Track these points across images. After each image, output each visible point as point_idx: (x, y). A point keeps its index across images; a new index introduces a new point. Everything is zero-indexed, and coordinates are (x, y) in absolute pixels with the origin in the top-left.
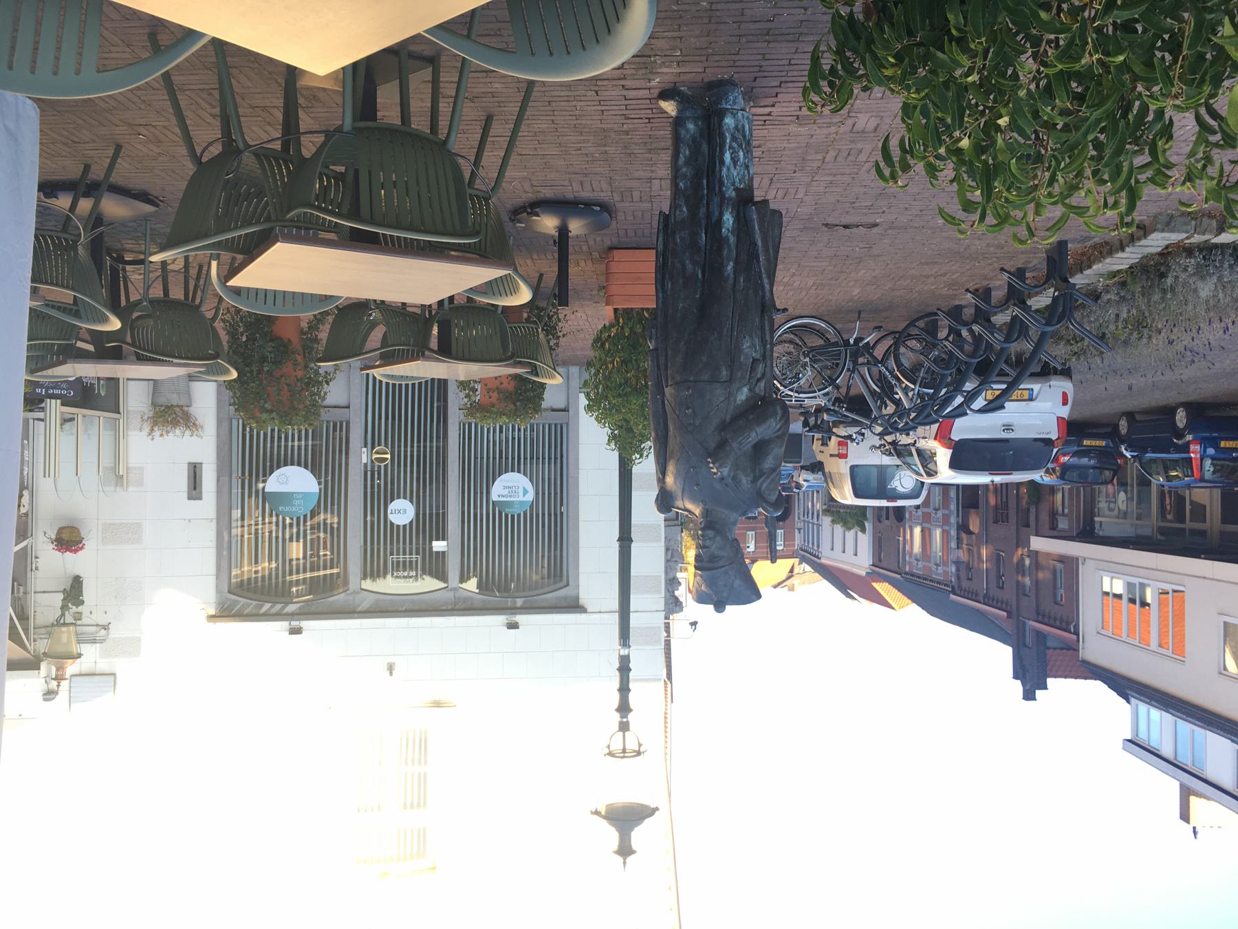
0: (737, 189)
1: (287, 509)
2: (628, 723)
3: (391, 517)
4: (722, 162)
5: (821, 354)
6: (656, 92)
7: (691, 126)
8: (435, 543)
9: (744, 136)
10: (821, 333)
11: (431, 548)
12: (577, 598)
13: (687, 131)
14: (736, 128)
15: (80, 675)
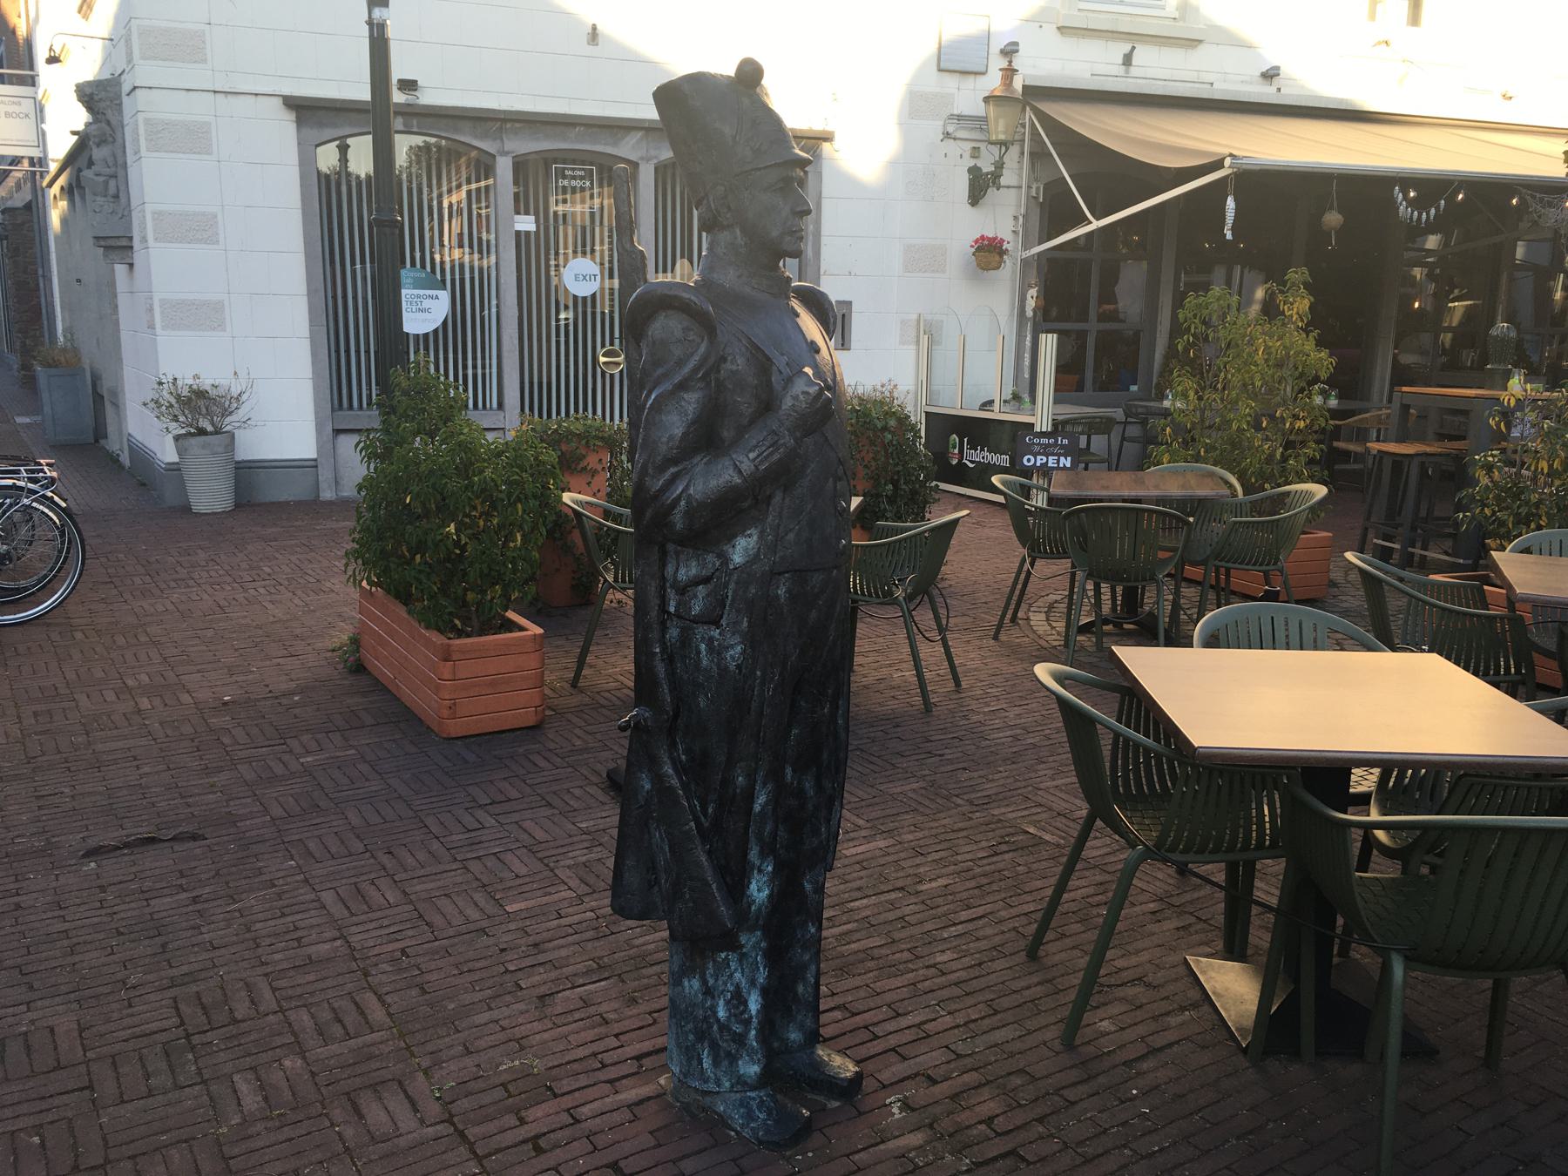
4: (765, 992)
6: (868, 1084)
7: (794, 1036)
8: (532, 227)
9: (714, 1047)
11: (537, 221)
12: (300, 122)
14: (733, 1059)
15: (976, 73)
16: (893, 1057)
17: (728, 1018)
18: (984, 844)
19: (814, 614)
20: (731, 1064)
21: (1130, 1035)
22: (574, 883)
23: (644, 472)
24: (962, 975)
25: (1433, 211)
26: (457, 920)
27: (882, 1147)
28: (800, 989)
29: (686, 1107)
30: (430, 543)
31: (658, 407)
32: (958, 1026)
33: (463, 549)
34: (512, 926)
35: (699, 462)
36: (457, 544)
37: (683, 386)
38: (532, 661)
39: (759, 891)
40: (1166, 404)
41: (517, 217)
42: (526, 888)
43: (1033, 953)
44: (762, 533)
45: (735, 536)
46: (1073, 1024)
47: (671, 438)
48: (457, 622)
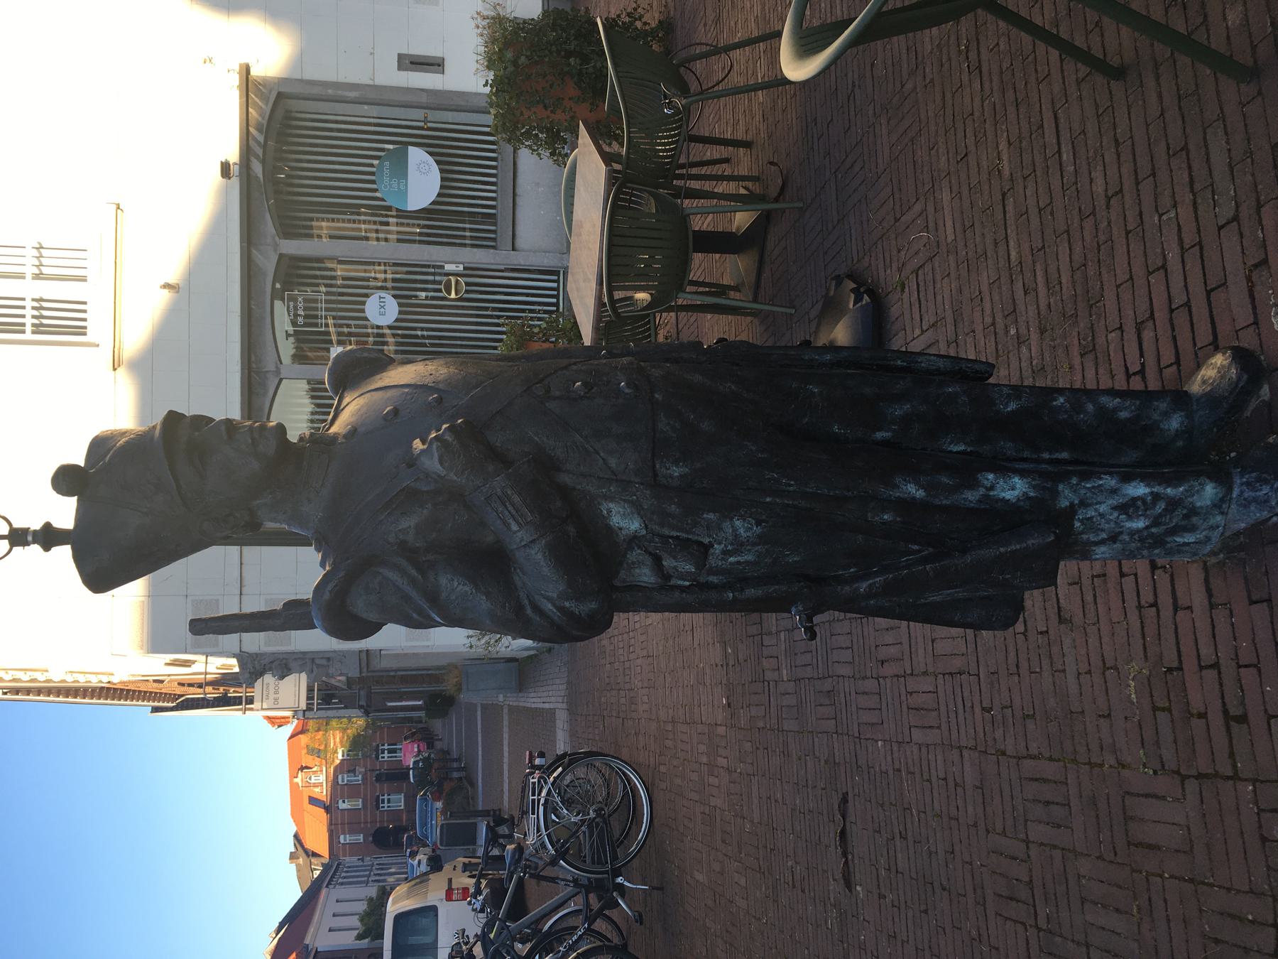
0: (1072, 510)
1: (386, 171)
2: (25, 543)
4: (1127, 478)
5: (601, 836)
6: (1248, 340)
7: (1175, 423)
9: (1174, 531)
10: (627, 834)
13: (1166, 414)
14: (1193, 511)
16: (1218, 297)
18: (965, 77)
19: (705, 426)
24: (1127, 169)
28: (1124, 415)
32: (1195, 203)
43: (1118, 73)
44: (607, 498)
45: (609, 529)
46: (1224, 64)
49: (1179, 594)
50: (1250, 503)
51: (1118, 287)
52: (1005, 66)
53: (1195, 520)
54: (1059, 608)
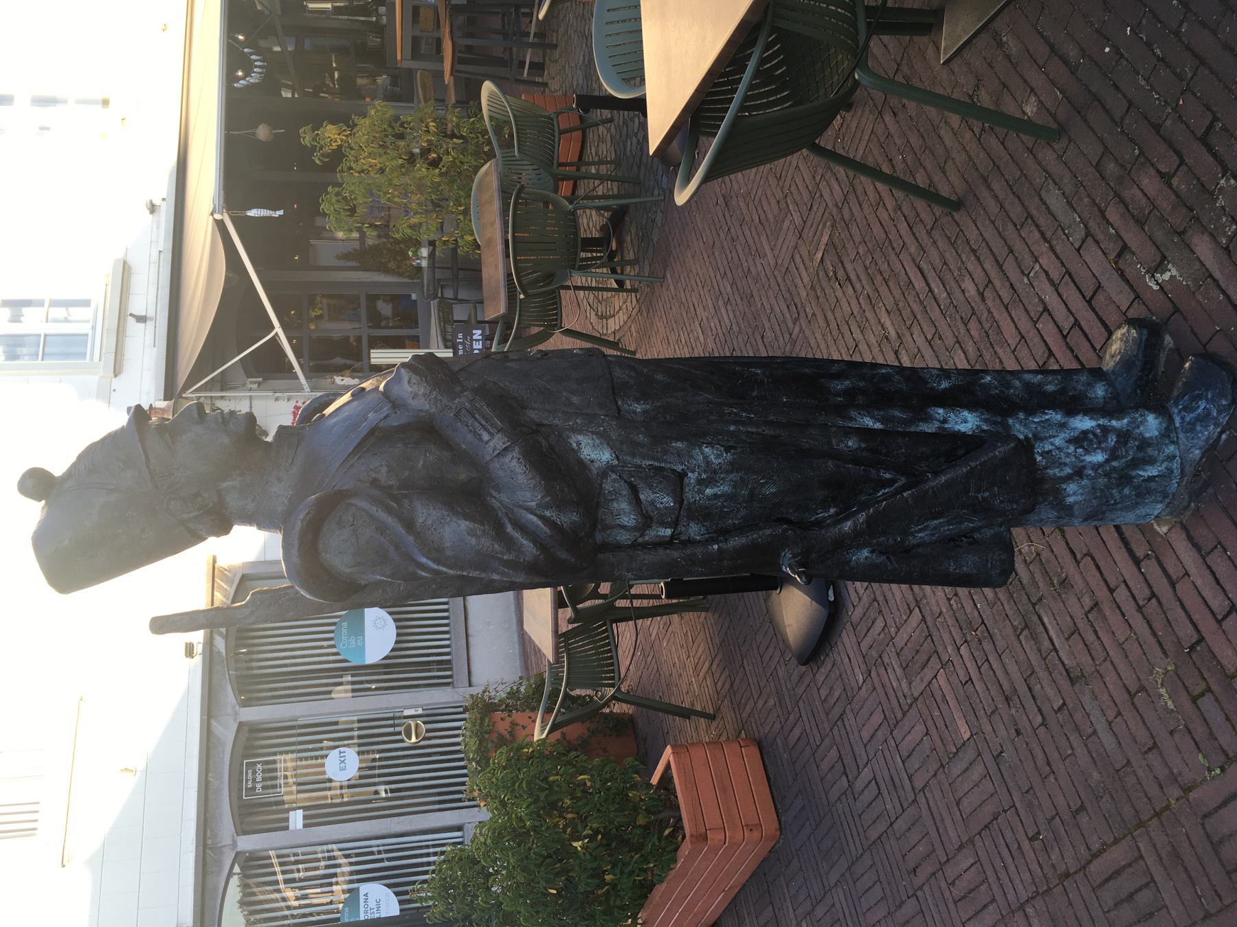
1: (344, 631)
3: (334, 754)
6: (1136, 312)
8: (300, 813)
9: (1136, 463)
11: (295, 809)
14: (1144, 444)
17: (1103, 450)
18: (839, 293)
19: (659, 377)
20: (1149, 445)
21: (1037, 79)
22: (928, 674)
23: (514, 565)
24: (989, 265)
25: (254, 57)
26: (987, 786)
27: (1217, 275)
28: (1050, 388)
29: (1195, 495)
30: (595, 865)
31: (437, 553)
32: (1052, 249)
33: (597, 832)
34: (987, 728)
35: (499, 499)
36: (592, 838)
37: (409, 525)
38: (698, 754)
39: (967, 422)
40: (424, 264)
41: (291, 827)
42: (940, 724)
43: (955, 205)
44: (576, 430)
45: (581, 462)
47: (471, 533)
48: (667, 832)
49: (1171, 571)
50: (1194, 425)
51: (1013, 352)
52: (868, 263)
53: (1150, 451)
54: (1067, 671)
